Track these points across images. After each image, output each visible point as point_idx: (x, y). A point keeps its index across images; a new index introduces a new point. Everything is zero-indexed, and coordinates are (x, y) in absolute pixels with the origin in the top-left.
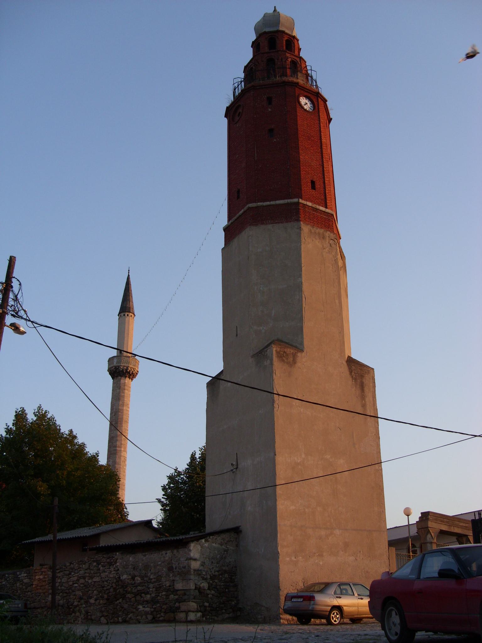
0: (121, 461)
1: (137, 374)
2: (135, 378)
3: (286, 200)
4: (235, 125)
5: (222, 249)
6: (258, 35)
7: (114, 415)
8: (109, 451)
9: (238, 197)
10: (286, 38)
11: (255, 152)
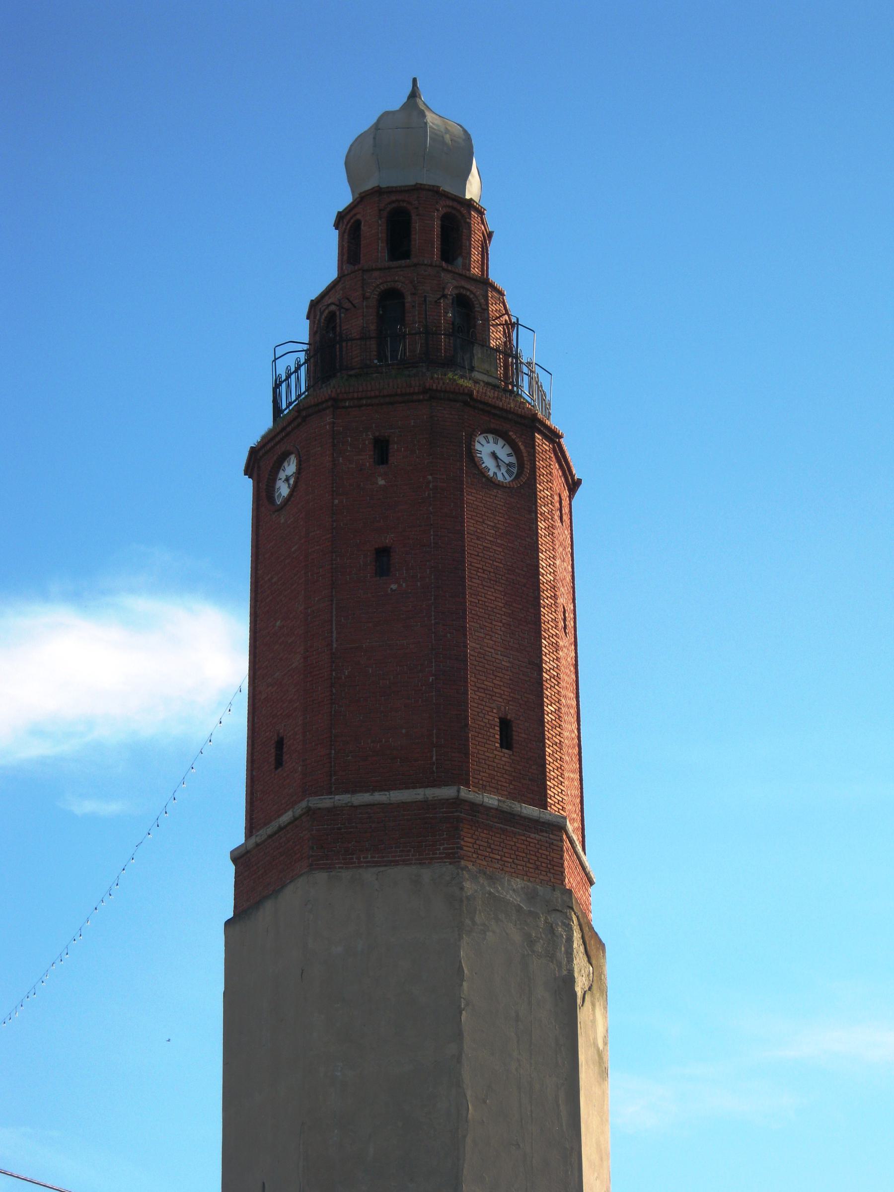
3: (421, 791)
4: (276, 514)
5: (228, 923)
6: (357, 196)
9: (279, 763)
10: (442, 211)
11: (332, 625)
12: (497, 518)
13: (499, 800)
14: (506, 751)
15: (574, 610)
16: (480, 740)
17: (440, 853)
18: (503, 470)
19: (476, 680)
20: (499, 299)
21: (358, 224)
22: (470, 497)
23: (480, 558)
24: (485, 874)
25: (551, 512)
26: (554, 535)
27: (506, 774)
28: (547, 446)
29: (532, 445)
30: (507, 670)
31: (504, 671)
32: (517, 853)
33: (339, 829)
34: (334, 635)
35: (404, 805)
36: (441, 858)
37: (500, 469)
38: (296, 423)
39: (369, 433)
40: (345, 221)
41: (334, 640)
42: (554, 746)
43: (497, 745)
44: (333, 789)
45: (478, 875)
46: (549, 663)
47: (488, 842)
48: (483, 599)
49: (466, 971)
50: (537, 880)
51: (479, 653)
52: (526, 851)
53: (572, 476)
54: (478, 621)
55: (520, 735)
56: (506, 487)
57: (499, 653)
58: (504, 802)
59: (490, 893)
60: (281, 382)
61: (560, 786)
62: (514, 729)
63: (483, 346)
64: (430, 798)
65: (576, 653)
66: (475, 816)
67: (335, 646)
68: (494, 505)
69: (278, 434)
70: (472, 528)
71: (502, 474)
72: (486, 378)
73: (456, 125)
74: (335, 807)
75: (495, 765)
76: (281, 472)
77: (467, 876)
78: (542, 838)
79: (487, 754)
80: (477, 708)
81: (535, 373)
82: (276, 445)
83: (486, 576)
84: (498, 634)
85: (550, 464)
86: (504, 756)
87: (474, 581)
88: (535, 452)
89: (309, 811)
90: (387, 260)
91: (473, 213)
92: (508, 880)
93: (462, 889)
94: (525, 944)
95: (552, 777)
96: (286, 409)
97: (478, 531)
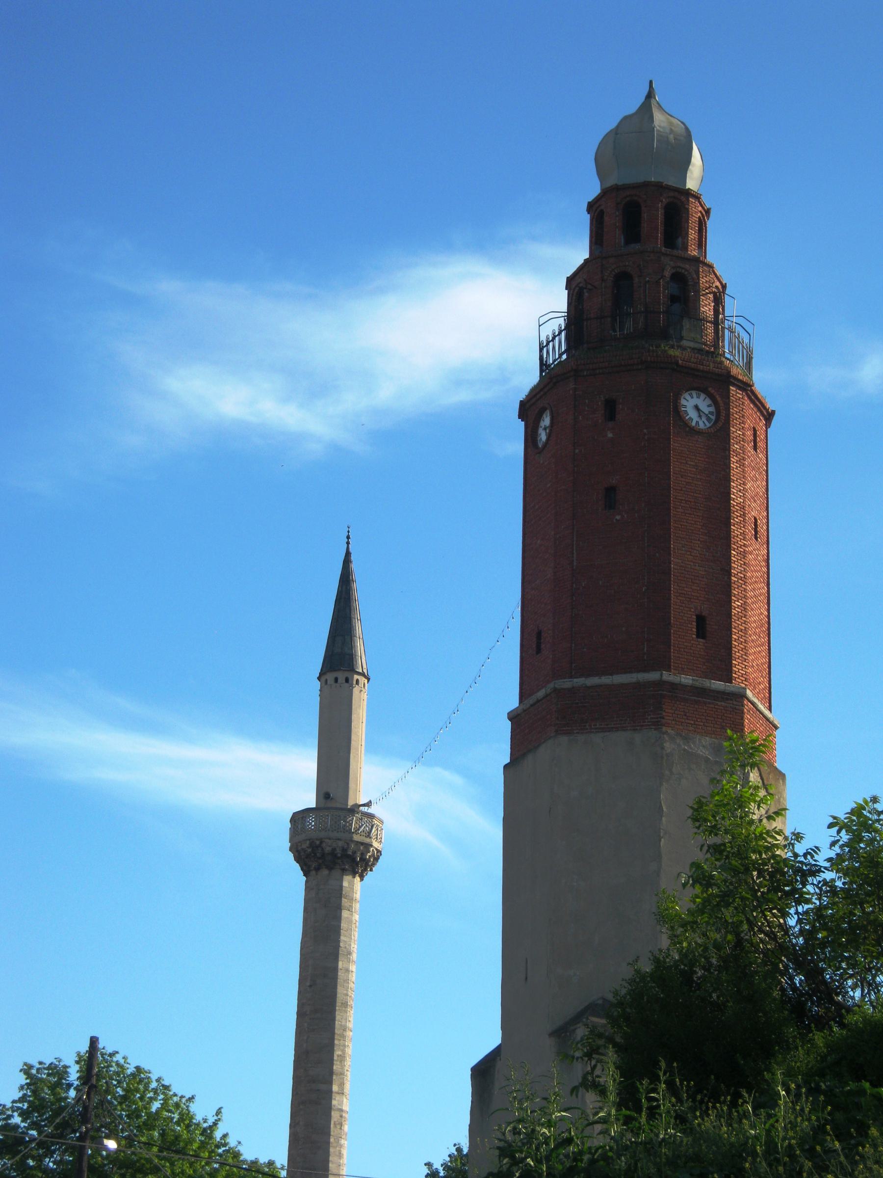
0: (332, 1123)
1: (376, 859)
2: (371, 870)
5: (506, 767)
7: (310, 986)
13: (693, 679)
14: (701, 640)
15: (768, 516)
16: (680, 633)
17: (648, 722)
18: (704, 419)
19: (678, 588)
20: (709, 272)
22: (676, 445)
24: (681, 736)
25: (743, 448)
28: (740, 394)
29: (727, 396)
30: (703, 578)
31: (700, 579)
33: (578, 703)
35: (622, 686)
37: (701, 418)
39: (601, 396)
43: (694, 636)
45: (676, 737)
46: (737, 568)
49: (665, 809)
53: (767, 410)
56: (705, 433)
57: (697, 565)
58: (697, 680)
59: (685, 750)
60: (543, 347)
61: (744, 663)
62: (708, 622)
65: (768, 550)
67: (575, 564)
70: (677, 469)
71: (703, 422)
72: (692, 345)
73: (679, 123)
76: (542, 422)
77: (667, 738)
78: (727, 705)
79: (685, 644)
83: (688, 506)
84: (697, 550)
85: (743, 409)
88: (729, 401)
89: (555, 690)
90: (622, 243)
91: (691, 199)
92: (699, 739)
93: (663, 748)
95: (737, 657)
96: (552, 364)
97: (682, 470)
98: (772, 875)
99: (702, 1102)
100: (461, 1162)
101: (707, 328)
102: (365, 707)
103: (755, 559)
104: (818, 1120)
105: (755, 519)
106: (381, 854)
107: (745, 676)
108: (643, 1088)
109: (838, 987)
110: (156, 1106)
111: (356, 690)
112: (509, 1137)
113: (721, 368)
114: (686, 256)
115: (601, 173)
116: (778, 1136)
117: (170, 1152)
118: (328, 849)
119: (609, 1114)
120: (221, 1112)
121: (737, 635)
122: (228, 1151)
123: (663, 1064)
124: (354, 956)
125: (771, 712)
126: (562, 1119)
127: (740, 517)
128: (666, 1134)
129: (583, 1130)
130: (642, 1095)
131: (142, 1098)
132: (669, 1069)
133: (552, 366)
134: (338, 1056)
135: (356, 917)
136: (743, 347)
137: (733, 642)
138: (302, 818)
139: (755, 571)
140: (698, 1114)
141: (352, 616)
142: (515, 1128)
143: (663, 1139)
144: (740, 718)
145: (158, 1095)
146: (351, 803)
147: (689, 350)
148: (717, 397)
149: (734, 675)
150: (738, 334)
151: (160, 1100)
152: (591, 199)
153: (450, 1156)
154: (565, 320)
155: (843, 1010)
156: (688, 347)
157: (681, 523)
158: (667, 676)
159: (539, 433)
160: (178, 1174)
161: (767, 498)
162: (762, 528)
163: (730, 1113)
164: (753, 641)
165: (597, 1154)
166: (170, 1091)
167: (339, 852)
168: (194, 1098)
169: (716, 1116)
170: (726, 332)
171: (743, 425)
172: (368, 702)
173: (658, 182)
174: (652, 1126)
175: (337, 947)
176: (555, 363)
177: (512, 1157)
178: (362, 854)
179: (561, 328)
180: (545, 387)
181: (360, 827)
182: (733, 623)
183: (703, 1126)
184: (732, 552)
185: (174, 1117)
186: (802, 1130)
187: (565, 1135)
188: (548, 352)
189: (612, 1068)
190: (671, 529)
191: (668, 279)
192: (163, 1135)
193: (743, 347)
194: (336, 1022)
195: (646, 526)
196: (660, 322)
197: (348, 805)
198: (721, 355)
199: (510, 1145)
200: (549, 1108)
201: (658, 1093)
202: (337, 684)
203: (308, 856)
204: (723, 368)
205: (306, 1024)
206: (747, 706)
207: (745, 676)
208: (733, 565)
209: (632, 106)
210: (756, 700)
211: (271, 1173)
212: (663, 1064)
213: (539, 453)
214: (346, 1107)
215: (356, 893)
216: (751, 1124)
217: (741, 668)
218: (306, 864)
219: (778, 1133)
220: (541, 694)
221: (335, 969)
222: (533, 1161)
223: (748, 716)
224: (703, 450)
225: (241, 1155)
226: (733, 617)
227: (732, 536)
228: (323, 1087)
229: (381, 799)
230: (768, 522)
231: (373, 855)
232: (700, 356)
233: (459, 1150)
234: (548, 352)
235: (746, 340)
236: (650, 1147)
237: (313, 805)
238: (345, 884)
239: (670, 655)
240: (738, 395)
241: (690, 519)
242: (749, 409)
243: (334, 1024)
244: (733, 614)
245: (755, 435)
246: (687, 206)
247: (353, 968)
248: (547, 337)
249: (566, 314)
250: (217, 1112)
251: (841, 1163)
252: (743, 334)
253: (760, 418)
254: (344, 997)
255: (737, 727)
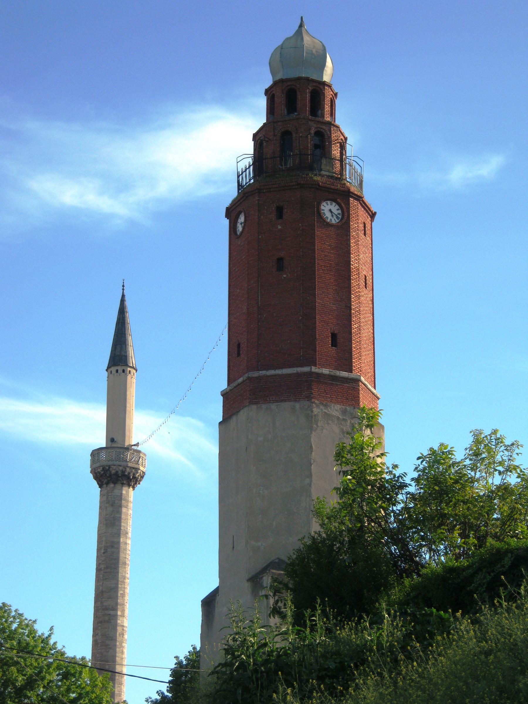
0: (118, 633)
1: (142, 477)
2: (139, 484)
5: (220, 423)
7: (104, 553)
8: (97, 617)
12: (331, 241)
13: (330, 371)
15: (372, 274)
16: (322, 344)
17: (303, 396)
18: (335, 217)
19: (320, 317)
21: (273, 95)
22: (319, 233)
23: (323, 261)
24: (323, 404)
25: (357, 234)
26: (359, 245)
27: (334, 358)
28: (356, 203)
29: (348, 204)
30: (335, 311)
31: (333, 312)
32: (338, 393)
33: (262, 386)
34: (260, 298)
35: (289, 375)
36: (304, 398)
37: (333, 217)
38: (243, 199)
40: (269, 93)
41: (260, 301)
42: (357, 343)
43: (330, 345)
44: (259, 368)
47: (325, 390)
48: (324, 279)
50: (347, 404)
51: (322, 304)
52: (342, 392)
53: (372, 212)
54: (322, 290)
55: (341, 340)
56: (336, 226)
58: (332, 371)
59: (325, 412)
61: (359, 361)
62: (338, 337)
63: (326, 158)
64: (299, 372)
65: (373, 294)
66: (319, 379)
67: (260, 304)
68: (330, 235)
69: (237, 203)
70: (319, 247)
72: (327, 173)
73: (319, 42)
74: (259, 376)
75: (329, 354)
76: (239, 219)
80: (321, 330)
81: (352, 166)
82: (237, 207)
85: (358, 211)
86: (333, 350)
87: (320, 271)
89: (249, 378)
90: (286, 114)
91: (326, 87)
93: (312, 412)
94: (341, 433)
95: (355, 357)
98: (379, 488)
99: (341, 621)
100: (196, 656)
101: (336, 164)
102: (135, 387)
103: (365, 300)
104: (406, 630)
105: (365, 276)
106: (145, 474)
107: (360, 369)
108: (307, 614)
109: (416, 553)
110: (14, 626)
111: (129, 377)
112: (231, 642)
113: (344, 187)
114: (323, 121)
115: (273, 73)
116: (384, 640)
117: (23, 653)
118: (113, 472)
119: (288, 629)
120: (53, 629)
121: (355, 344)
122: (57, 652)
123: (319, 601)
124: (130, 535)
125: (375, 389)
126: (261, 632)
127: (356, 275)
128: (320, 640)
129: (273, 639)
130: (307, 618)
131: (6, 621)
132: (323, 603)
133: (245, 187)
134: (121, 594)
135: (131, 512)
136: (357, 174)
137: (353, 349)
138: (98, 453)
139: (366, 307)
140: (338, 629)
141: (126, 333)
142: (234, 638)
143: (319, 643)
144: (358, 393)
145: (16, 620)
146: (127, 444)
147: (325, 177)
148: (342, 204)
149: (353, 368)
150: (355, 167)
151: (17, 622)
152: (267, 87)
153: (189, 652)
154: (252, 159)
155: (419, 566)
156: (325, 175)
157: (322, 279)
158: (314, 369)
159: (238, 226)
160: (29, 666)
161: (372, 264)
162: (369, 281)
163: (356, 628)
164: (364, 348)
165: (282, 652)
166: (23, 617)
167: (120, 473)
168: (36, 621)
169: (349, 629)
170: (347, 166)
171: (357, 221)
172: (136, 384)
173: (307, 77)
174: (312, 635)
175: (120, 529)
176: (247, 185)
177: (233, 654)
178: (134, 474)
179: (250, 164)
180: (241, 199)
181: (132, 458)
182: (353, 338)
183: (341, 635)
184: (352, 296)
185: (25, 633)
186: (397, 636)
187: (263, 641)
188: (242, 178)
189: (290, 603)
190: (316, 282)
191: (313, 135)
192: (19, 643)
193: (357, 174)
194: (120, 574)
195: (301, 281)
196: (308, 161)
197: (125, 445)
198: (344, 180)
199: (231, 648)
200: (253, 626)
201: (316, 617)
202: (117, 374)
203: (101, 476)
204: (346, 187)
205: (101, 576)
206: (361, 386)
207: (360, 369)
208: (352, 303)
209: (291, 31)
210: (366, 383)
211: (83, 664)
212: (319, 601)
213: (238, 238)
214: (126, 624)
215: (130, 498)
216: (368, 634)
217: (357, 364)
218: (100, 481)
219: (384, 638)
220: (240, 380)
221: (119, 543)
222: (245, 656)
223: (362, 392)
224: (334, 236)
225: (66, 654)
226: (353, 334)
227: (352, 286)
228: (112, 612)
229: (145, 442)
230: (373, 278)
231: (140, 474)
232: (332, 180)
233: (194, 648)
234: (242, 178)
235: (359, 171)
236: (311, 647)
237: (104, 445)
238: (124, 492)
239: (316, 357)
240: (354, 203)
241: (327, 276)
242: (361, 211)
243: (118, 575)
244: (353, 332)
245: (365, 227)
246: (323, 91)
247: (129, 542)
248: (242, 169)
249: (253, 156)
250: (50, 629)
251: (420, 656)
252: (357, 167)
253: (367, 217)
254: (124, 559)
255: (355, 398)
